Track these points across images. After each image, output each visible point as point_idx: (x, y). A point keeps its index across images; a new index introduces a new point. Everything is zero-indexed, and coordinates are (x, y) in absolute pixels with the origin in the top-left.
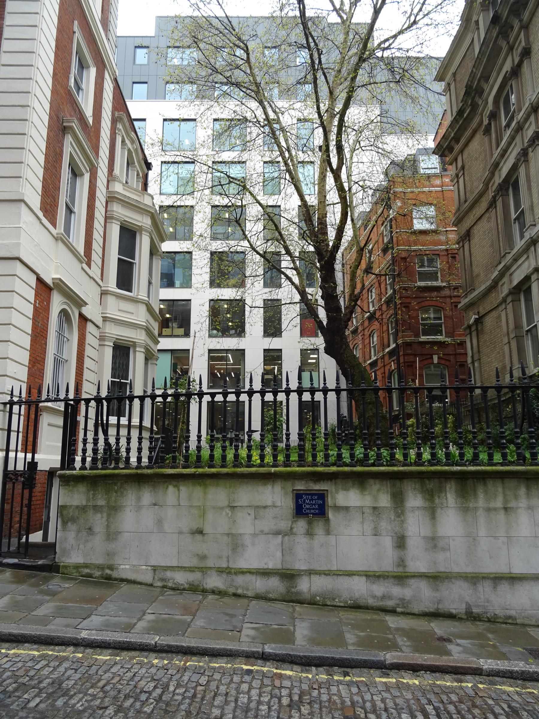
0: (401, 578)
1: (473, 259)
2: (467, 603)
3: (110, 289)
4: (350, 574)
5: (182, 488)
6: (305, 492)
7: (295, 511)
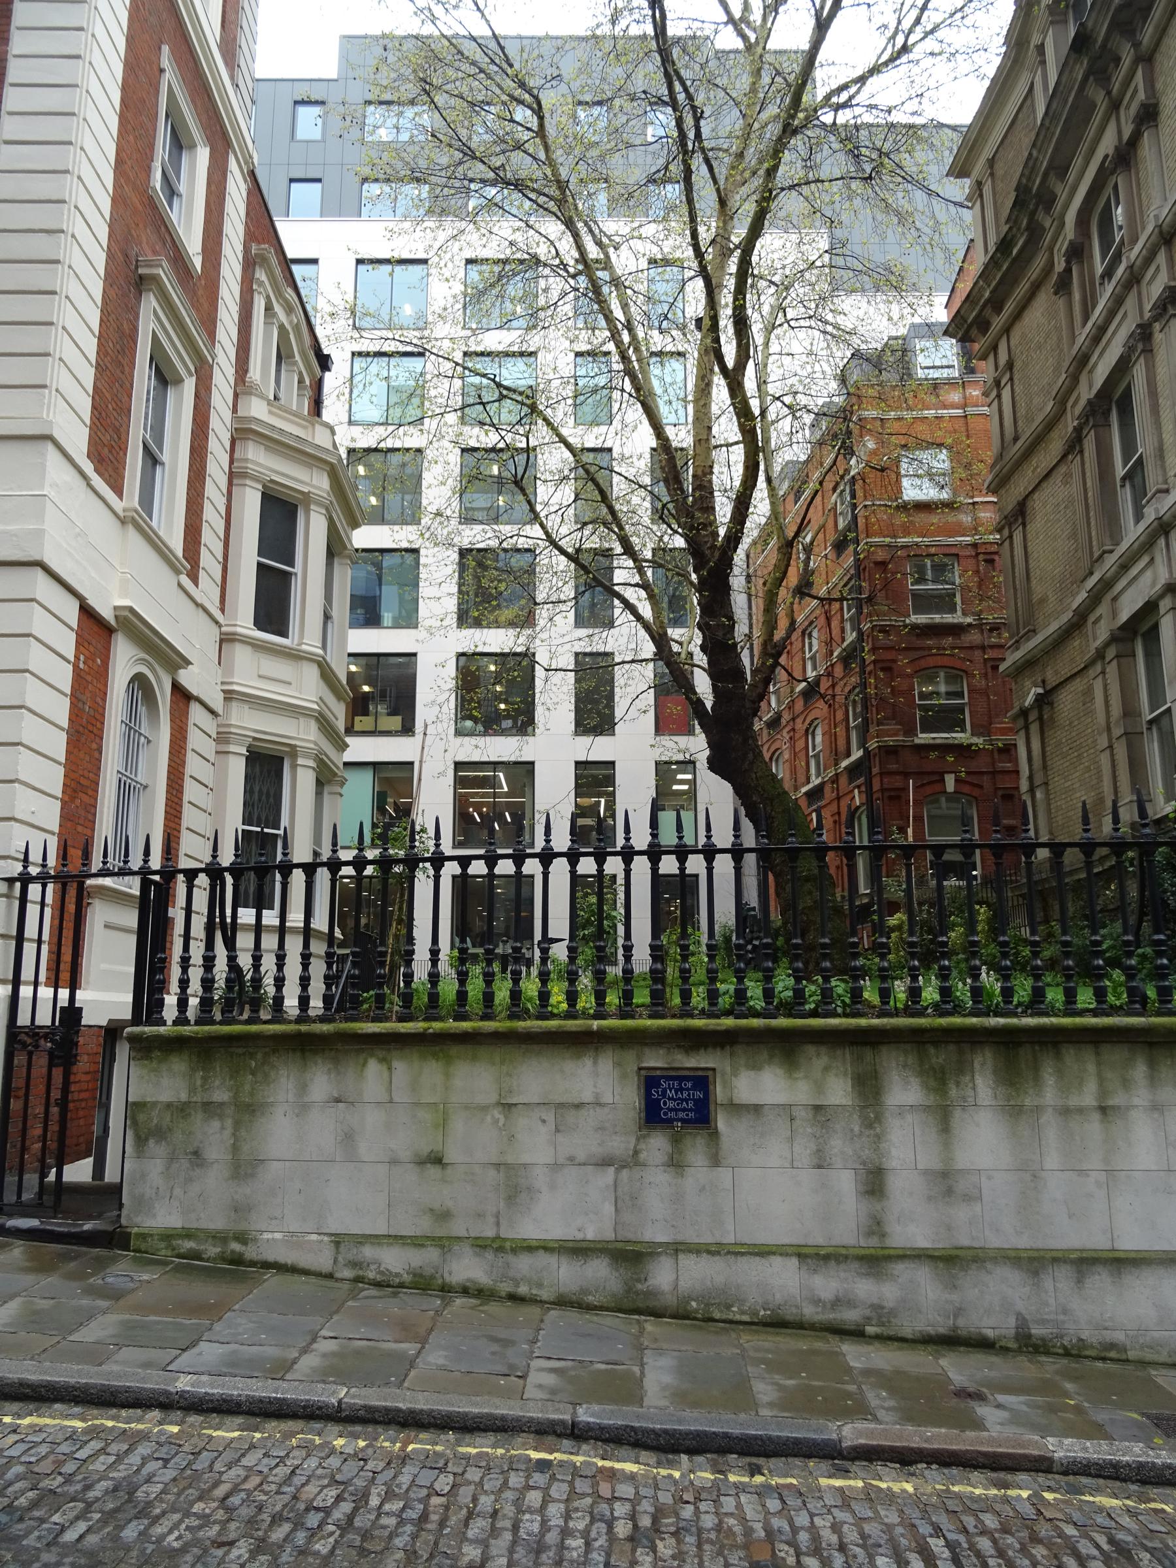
0: (876, 1260)
1: (1032, 564)
2: (1019, 1315)
3: (239, 630)
4: (763, 1252)
5: (396, 1064)
6: (665, 1073)
7: (643, 1115)
